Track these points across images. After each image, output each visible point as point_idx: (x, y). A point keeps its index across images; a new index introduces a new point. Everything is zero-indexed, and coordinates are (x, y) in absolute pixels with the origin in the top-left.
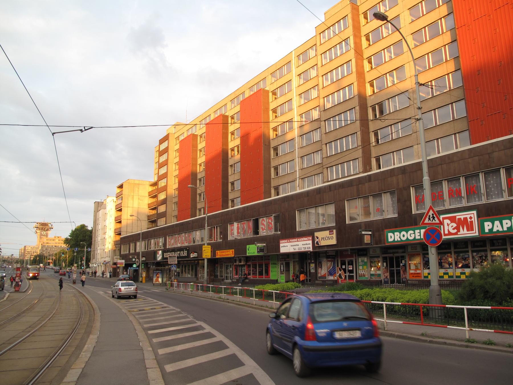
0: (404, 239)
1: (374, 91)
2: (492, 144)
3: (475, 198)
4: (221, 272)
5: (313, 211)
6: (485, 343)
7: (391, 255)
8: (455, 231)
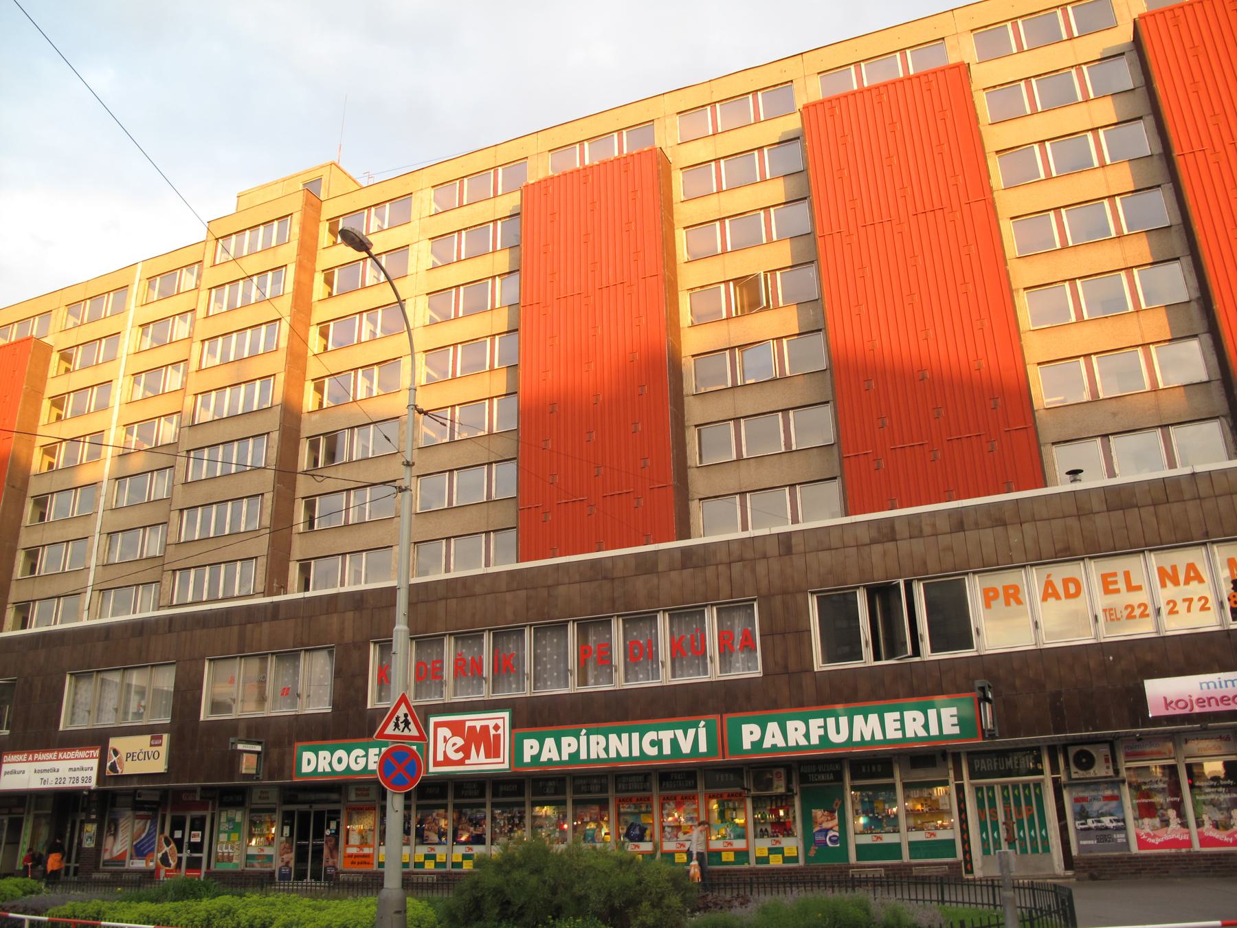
0: (339, 768)
1: (321, 404)
2: (557, 567)
3: (510, 685)
5: (115, 678)
7: (305, 807)
8: (460, 755)
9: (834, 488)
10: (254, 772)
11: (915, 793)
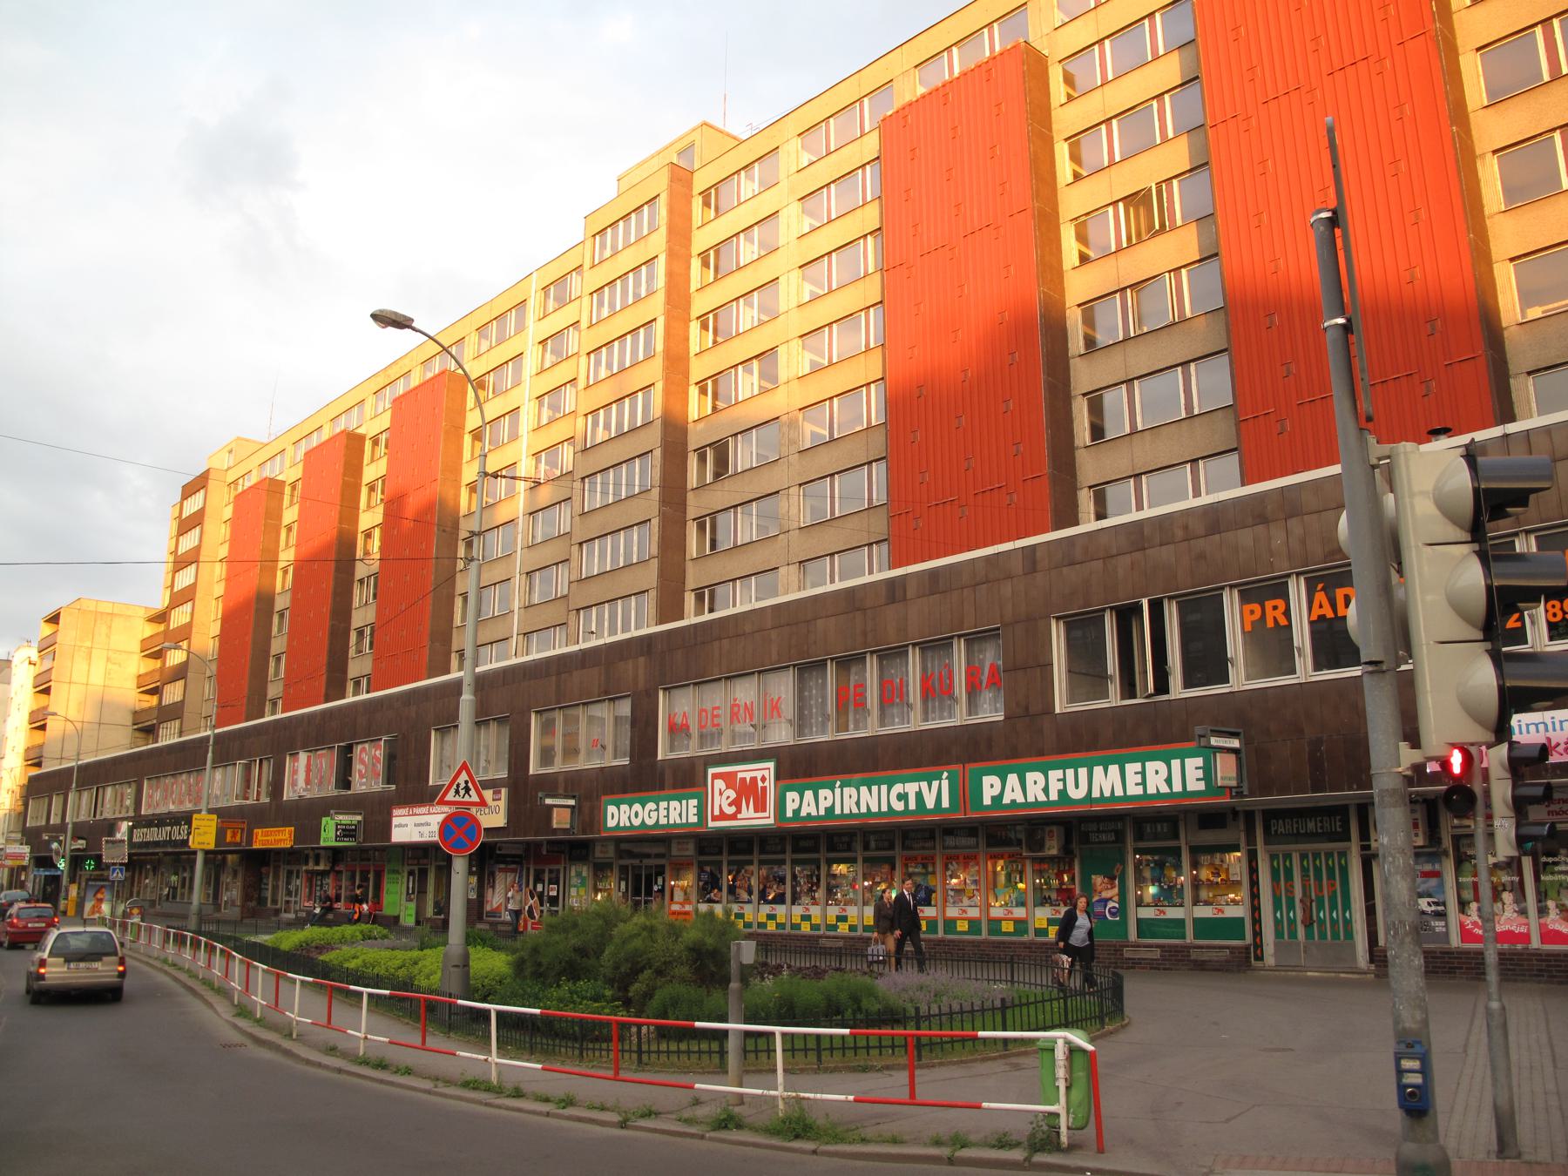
4: (275, 888)
6: (466, 1085)
8: (732, 810)
9: (1234, 459)
10: (1234, 783)
11: (1205, 859)
